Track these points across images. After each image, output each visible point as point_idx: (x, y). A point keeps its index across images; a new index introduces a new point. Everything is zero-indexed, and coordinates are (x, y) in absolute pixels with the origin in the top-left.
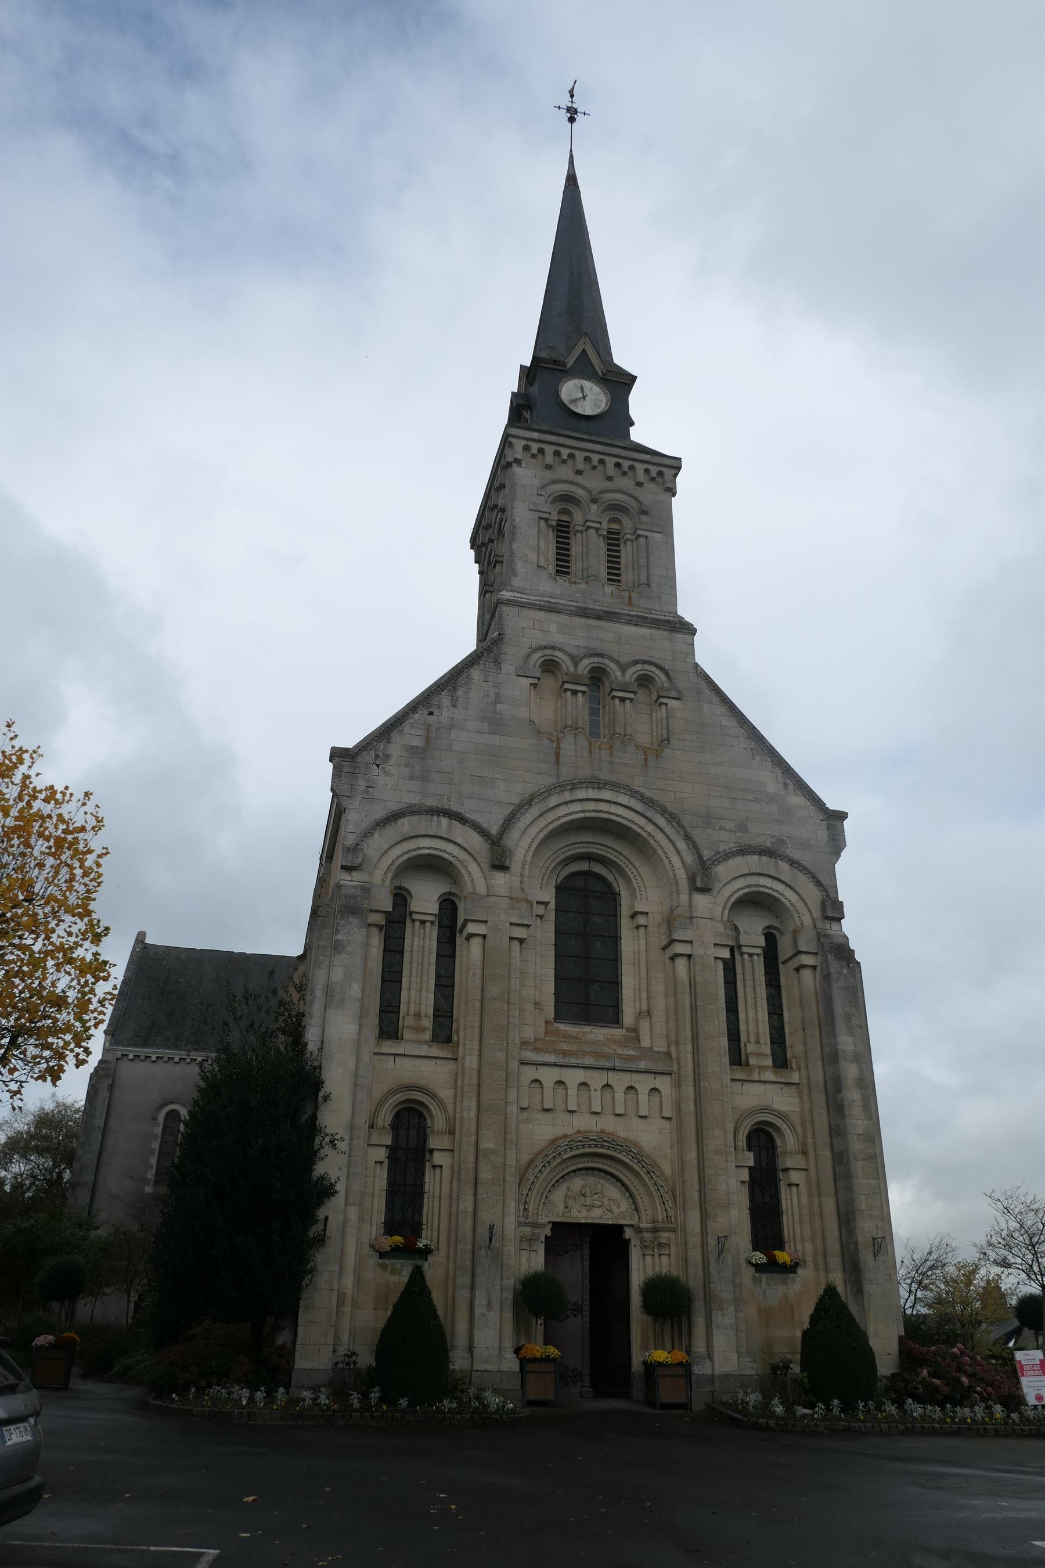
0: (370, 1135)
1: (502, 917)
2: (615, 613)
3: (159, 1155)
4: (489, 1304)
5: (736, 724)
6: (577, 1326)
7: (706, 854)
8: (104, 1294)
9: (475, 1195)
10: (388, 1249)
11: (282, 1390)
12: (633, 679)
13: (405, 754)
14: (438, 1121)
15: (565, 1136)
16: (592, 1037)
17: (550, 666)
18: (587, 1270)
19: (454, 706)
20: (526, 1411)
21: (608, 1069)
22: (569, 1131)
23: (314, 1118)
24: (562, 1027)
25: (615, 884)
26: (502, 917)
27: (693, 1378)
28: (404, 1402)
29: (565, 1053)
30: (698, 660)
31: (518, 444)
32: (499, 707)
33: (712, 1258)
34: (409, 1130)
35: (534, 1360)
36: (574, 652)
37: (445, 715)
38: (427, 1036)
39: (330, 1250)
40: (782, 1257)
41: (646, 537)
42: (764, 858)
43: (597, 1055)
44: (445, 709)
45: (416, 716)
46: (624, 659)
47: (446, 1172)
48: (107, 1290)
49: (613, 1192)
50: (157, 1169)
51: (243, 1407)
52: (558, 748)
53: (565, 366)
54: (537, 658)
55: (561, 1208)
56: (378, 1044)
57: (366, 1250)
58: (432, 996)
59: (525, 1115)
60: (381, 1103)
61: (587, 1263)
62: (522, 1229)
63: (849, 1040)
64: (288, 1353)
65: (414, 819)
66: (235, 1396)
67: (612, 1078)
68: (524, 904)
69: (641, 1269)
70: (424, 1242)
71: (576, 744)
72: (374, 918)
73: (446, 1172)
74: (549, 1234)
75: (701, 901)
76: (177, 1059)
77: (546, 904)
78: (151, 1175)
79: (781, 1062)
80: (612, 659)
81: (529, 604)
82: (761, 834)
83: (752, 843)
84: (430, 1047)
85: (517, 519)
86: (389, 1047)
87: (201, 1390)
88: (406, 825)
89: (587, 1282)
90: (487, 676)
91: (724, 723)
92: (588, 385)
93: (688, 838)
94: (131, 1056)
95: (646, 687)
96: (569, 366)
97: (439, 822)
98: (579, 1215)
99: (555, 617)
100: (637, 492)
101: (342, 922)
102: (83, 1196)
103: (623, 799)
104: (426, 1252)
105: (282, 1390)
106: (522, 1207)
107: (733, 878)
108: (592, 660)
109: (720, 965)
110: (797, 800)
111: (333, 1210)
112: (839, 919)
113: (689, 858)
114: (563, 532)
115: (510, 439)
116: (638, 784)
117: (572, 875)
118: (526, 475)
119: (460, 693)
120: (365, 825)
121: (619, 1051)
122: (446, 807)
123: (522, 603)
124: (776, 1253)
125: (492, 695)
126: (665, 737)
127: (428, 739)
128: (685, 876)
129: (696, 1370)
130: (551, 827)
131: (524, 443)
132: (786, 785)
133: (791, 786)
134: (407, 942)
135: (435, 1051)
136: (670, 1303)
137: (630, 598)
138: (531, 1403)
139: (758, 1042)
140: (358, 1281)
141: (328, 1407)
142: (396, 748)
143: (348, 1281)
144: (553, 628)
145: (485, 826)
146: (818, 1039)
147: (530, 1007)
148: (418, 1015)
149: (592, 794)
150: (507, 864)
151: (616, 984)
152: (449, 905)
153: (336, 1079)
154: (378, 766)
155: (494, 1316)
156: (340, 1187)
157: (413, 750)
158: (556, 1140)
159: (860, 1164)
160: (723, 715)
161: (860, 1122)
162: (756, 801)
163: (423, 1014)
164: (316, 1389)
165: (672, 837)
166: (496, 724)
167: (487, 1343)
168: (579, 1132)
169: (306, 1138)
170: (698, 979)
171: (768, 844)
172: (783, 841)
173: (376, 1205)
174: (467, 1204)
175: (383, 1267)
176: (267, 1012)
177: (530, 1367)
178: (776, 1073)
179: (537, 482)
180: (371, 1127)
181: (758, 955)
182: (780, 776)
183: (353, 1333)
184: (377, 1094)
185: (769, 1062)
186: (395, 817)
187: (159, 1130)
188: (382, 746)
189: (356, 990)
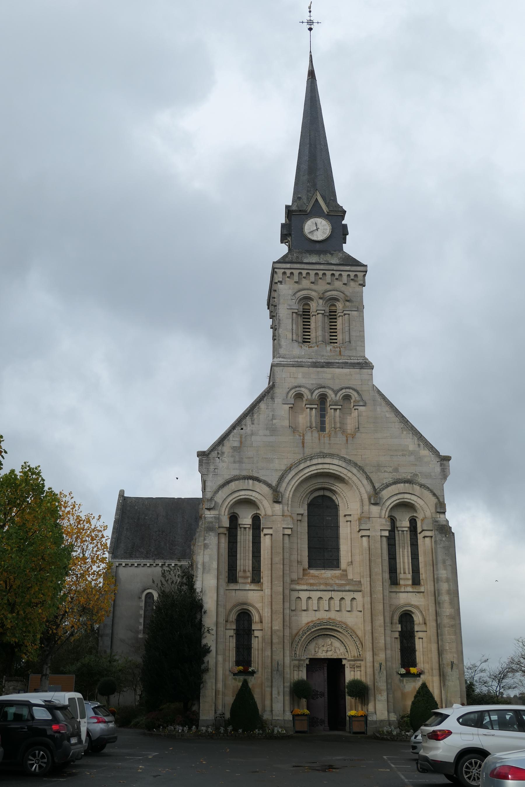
0: (226, 625)
1: (279, 526)
2: (332, 363)
3: (144, 617)
4: (279, 693)
5: (394, 415)
6: (322, 702)
7: (377, 485)
8: (123, 691)
9: (272, 648)
10: (237, 672)
11: (194, 727)
12: (340, 398)
13: (231, 451)
14: (256, 618)
15: (312, 621)
16: (324, 576)
17: (299, 396)
18: (326, 678)
19: (253, 424)
20: (295, 734)
21: (332, 591)
22: (314, 619)
23: (201, 620)
24: (313, 572)
25: (336, 501)
26: (279, 526)
27: (368, 722)
28: (240, 731)
29: (311, 585)
30: (375, 383)
31: (280, 272)
32: (274, 421)
33: (377, 672)
34: (243, 621)
35: (298, 715)
36: (311, 387)
37: (249, 429)
38: (249, 580)
39: (212, 673)
40: (413, 670)
41: (349, 314)
42: (406, 485)
43: (326, 584)
44: (248, 426)
45: (235, 431)
46: (336, 388)
47: (260, 639)
48: (125, 690)
49: (337, 644)
50: (144, 625)
51: (179, 733)
52: (303, 439)
53: (306, 212)
54: (292, 393)
55: (313, 652)
56: (228, 586)
57: (228, 672)
58: (251, 562)
59: (294, 613)
60: (231, 611)
61: (326, 675)
62: (294, 662)
63: (444, 572)
64: (197, 714)
65: (237, 482)
66: (177, 729)
67: (333, 594)
68: (289, 518)
69: (349, 676)
70: (252, 668)
71: (312, 436)
72: (222, 530)
73: (260, 639)
74: (308, 663)
75: (375, 510)
76: (148, 565)
77: (302, 515)
78: (141, 627)
79: (416, 581)
80: (329, 388)
81: (287, 364)
82: (405, 472)
83: (400, 477)
84: (250, 585)
85: (281, 315)
86: (232, 586)
87: (164, 728)
88: (233, 486)
89: (326, 683)
90: (268, 406)
91: (387, 416)
92: (319, 220)
93: (368, 478)
94: (124, 565)
95: (349, 399)
96: (308, 211)
97: (248, 483)
98: (321, 655)
99: (301, 369)
100: (344, 288)
101: (207, 535)
102: (107, 641)
103: (336, 462)
104: (253, 673)
105: (194, 727)
106: (293, 653)
107: (390, 496)
108: (320, 390)
109: (384, 540)
110: (425, 452)
111: (210, 659)
112: (444, 513)
113: (369, 488)
114: (305, 315)
115: (276, 270)
116: (343, 453)
117: (315, 498)
118: (286, 289)
119: (255, 416)
120: (215, 487)
121: (337, 582)
122: (251, 475)
123: (284, 364)
124: (411, 669)
125: (271, 415)
126: (357, 427)
127: (241, 442)
128: (367, 497)
129: (369, 719)
130: (301, 479)
131: (283, 270)
132: (419, 445)
133: (422, 445)
134: (239, 537)
135: (253, 587)
136: (361, 692)
137: (340, 351)
138: (297, 732)
139: (405, 573)
140: (225, 685)
141: (211, 733)
142: (226, 448)
143: (220, 686)
144: (300, 376)
145: (270, 482)
146: (432, 571)
147: (295, 564)
148: (244, 571)
149: (320, 461)
150: (280, 500)
151: (338, 549)
152: (256, 519)
153: (210, 603)
154: (219, 458)
155: (281, 698)
156: (213, 649)
157: (234, 449)
158: (308, 623)
159: (446, 629)
160: (387, 412)
161: (448, 610)
162: (403, 455)
163: (247, 570)
164: (208, 727)
165: (360, 479)
166: (273, 430)
167: (277, 707)
168: (319, 619)
169: (198, 628)
170: (373, 547)
171: (409, 477)
172: (417, 475)
173: (231, 654)
174: (268, 653)
175: (235, 679)
176: (179, 577)
177: (296, 718)
178: (413, 588)
179: (291, 292)
180: (227, 621)
181: (407, 531)
182: (416, 441)
183: (224, 706)
184: (229, 607)
185: (410, 582)
186: (228, 482)
187: (143, 604)
188: (220, 448)
189: (215, 565)
